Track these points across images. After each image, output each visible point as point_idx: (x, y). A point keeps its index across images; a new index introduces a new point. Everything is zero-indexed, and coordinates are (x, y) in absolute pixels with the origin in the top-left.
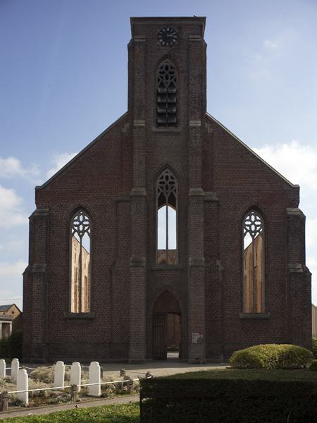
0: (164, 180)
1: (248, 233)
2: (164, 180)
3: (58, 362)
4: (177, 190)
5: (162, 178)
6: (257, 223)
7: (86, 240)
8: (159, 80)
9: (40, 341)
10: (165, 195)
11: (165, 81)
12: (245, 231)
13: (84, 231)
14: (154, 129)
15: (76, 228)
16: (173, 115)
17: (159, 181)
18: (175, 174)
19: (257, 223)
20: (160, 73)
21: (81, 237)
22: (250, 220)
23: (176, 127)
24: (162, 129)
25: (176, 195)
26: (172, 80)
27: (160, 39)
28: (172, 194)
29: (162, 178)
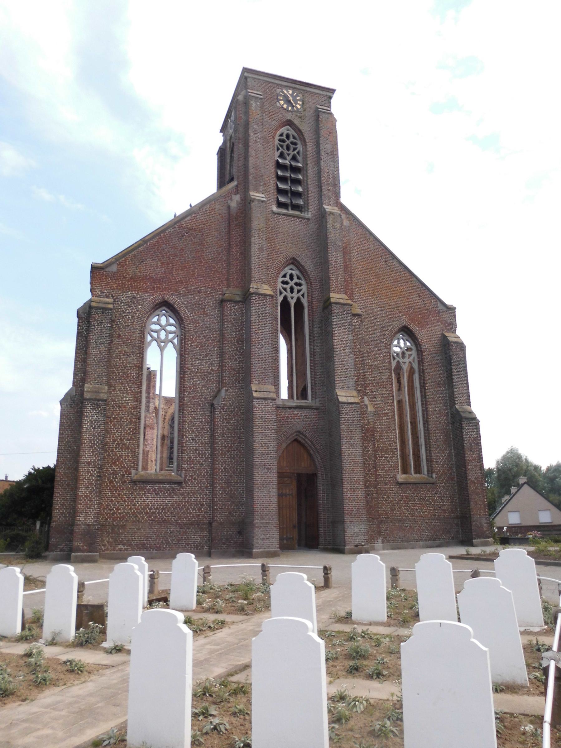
0: (287, 279)
1: (154, 343)
2: (287, 279)
3: (179, 556)
4: (306, 295)
5: (284, 276)
6: (169, 328)
7: (171, 355)
8: (278, 149)
9: (91, 520)
10: (289, 299)
11: (286, 152)
12: (149, 338)
13: (166, 342)
14: (275, 209)
15: (155, 335)
16: (298, 195)
17: (280, 280)
18: (301, 271)
19: (169, 328)
20: (280, 140)
21: (162, 349)
22: (158, 323)
23: (301, 211)
24: (283, 211)
25: (305, 301)
26: (295, 152)
27: (281, 100)
28: (298, 299)
29: (284, 276)
